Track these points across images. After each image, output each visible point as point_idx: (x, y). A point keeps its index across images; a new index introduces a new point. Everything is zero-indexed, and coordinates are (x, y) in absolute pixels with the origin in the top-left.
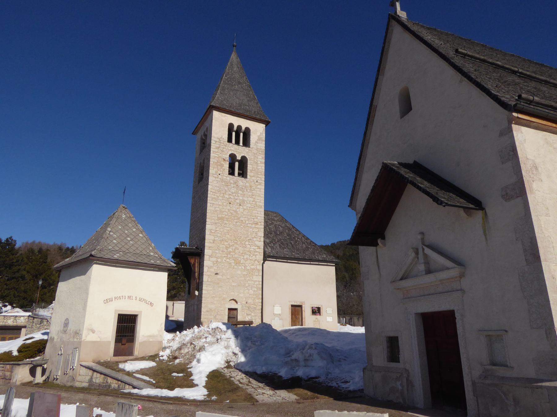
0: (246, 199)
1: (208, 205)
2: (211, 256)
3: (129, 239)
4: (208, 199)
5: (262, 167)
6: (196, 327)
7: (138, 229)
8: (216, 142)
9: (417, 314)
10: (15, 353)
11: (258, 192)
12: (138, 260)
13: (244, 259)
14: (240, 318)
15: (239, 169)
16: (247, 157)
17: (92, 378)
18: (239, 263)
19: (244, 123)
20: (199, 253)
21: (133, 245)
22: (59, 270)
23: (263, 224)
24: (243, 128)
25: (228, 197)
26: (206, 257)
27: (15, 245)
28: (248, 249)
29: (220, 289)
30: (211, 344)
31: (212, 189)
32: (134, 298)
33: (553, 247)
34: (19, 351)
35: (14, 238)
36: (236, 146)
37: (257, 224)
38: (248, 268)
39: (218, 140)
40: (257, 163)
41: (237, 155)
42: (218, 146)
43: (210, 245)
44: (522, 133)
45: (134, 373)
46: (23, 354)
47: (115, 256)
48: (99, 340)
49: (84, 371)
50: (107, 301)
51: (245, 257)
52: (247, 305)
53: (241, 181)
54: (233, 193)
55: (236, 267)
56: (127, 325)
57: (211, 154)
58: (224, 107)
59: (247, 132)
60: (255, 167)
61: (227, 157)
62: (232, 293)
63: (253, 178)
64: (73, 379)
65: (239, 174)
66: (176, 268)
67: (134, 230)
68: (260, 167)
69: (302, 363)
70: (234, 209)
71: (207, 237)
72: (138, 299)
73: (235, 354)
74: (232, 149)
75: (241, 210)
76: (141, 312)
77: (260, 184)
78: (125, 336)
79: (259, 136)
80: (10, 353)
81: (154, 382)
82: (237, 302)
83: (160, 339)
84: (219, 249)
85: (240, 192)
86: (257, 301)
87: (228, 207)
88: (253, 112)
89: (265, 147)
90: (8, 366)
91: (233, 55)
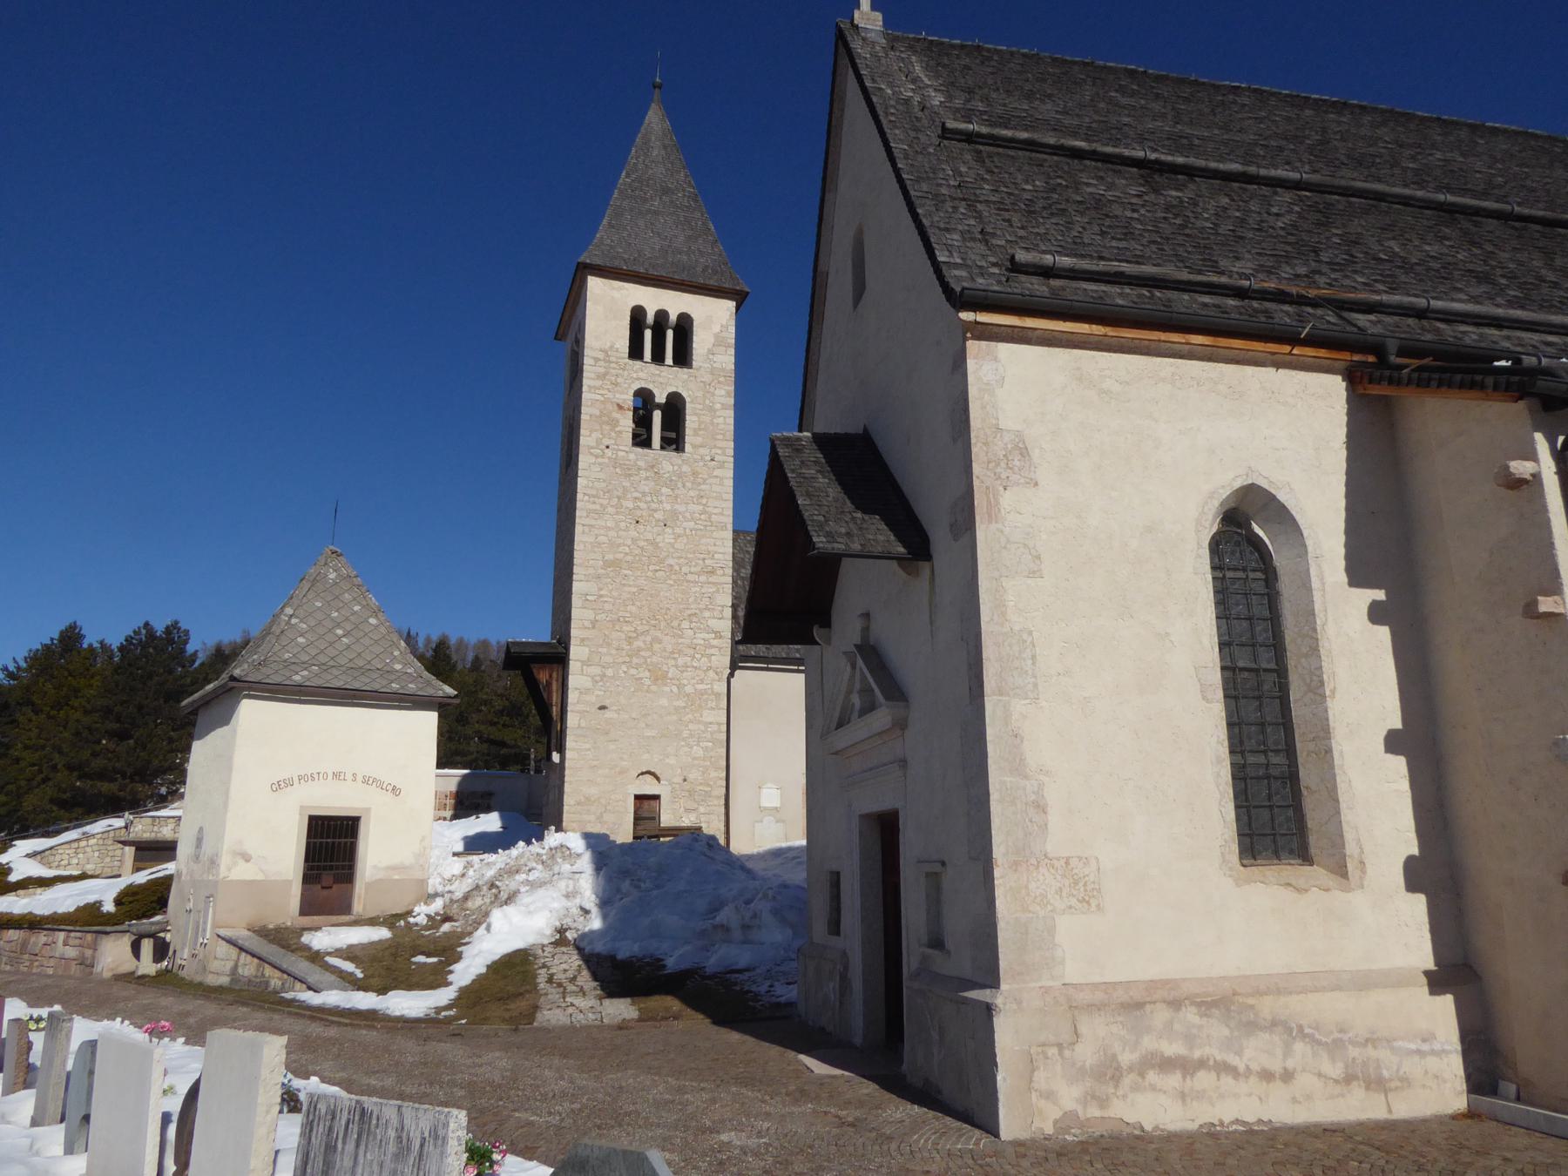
0: (681, 508)
1: (578, 529)
2: (586, 663)
3: (340, 632)
4: (578, 513)
5: (726, 420)
6: (521, 844)
7: (366, 607)
8: (597, 360)
9: (865, 817)
10: (109, 907)
11: (717, 488)
12: (357, 685)
13: (676, 666)
14: (667, 819)
15: (664, 427)
16: (684, 394)
17: (236, 967)
18: (665, 676)
19: (675, 303)
20: (556, 656)
21: (348, 647)
22: (194, 712)
23: (730, 571)
24: (673, 317)
25: (631, 505)
26: (574, 666)
27: (186, 642)
28: (687, 641)
29: (612, 747)
30: (534, 885)
31: (586, 487)
32: (349, 777)
33: (1034, 657)
34: (118, 901)
35: (183, 625)
36: (654, 368)
37: (712, 572)
38: (689, 689)
39: (601, 355)
40: (712, 409)
41: (656, 391)
42: (602, 370)
43: (586, 634)
44: (996, 359)
45: (329, 954)
46: (126, 908)
47: (297, 678)
48: (260, 877)
49: (223, 949)
50: (278, 786)
51: (680, 661)
52: (687, 786)
53: (668, 461)
54: (644, 494)
55: (654, 688)
56: (331, 845)
57: (584, 395)
58: (616, 263)
59: (684, 328)
60: (707, 419)
61: (628, 399)
62: (646, 756)
63: (702, 451)
64: (204, 968)
65: (667, 443)
66: (457, 701)
67: (356, 608)
68: (721, 420)
69: (737, 934)
70: (650, 537)
71: (575, 613)
72: (360, 778)
73: (586, 912)
74: (641, 374)
75: (669, 539)
76: (368, 810)
77: (722, 465)
78: (331, 868)
79: (716, 336)
80: (97, 905)
81: (360, 975)
82: (658, 779)
83: (418, 875)
84: (609, 645)
85: (664, 490)
86: (713, 774)
87: (634, 534)
88: (699, 269)
89: (736, 364)
90: (89, 937)
91: (650, 113)
